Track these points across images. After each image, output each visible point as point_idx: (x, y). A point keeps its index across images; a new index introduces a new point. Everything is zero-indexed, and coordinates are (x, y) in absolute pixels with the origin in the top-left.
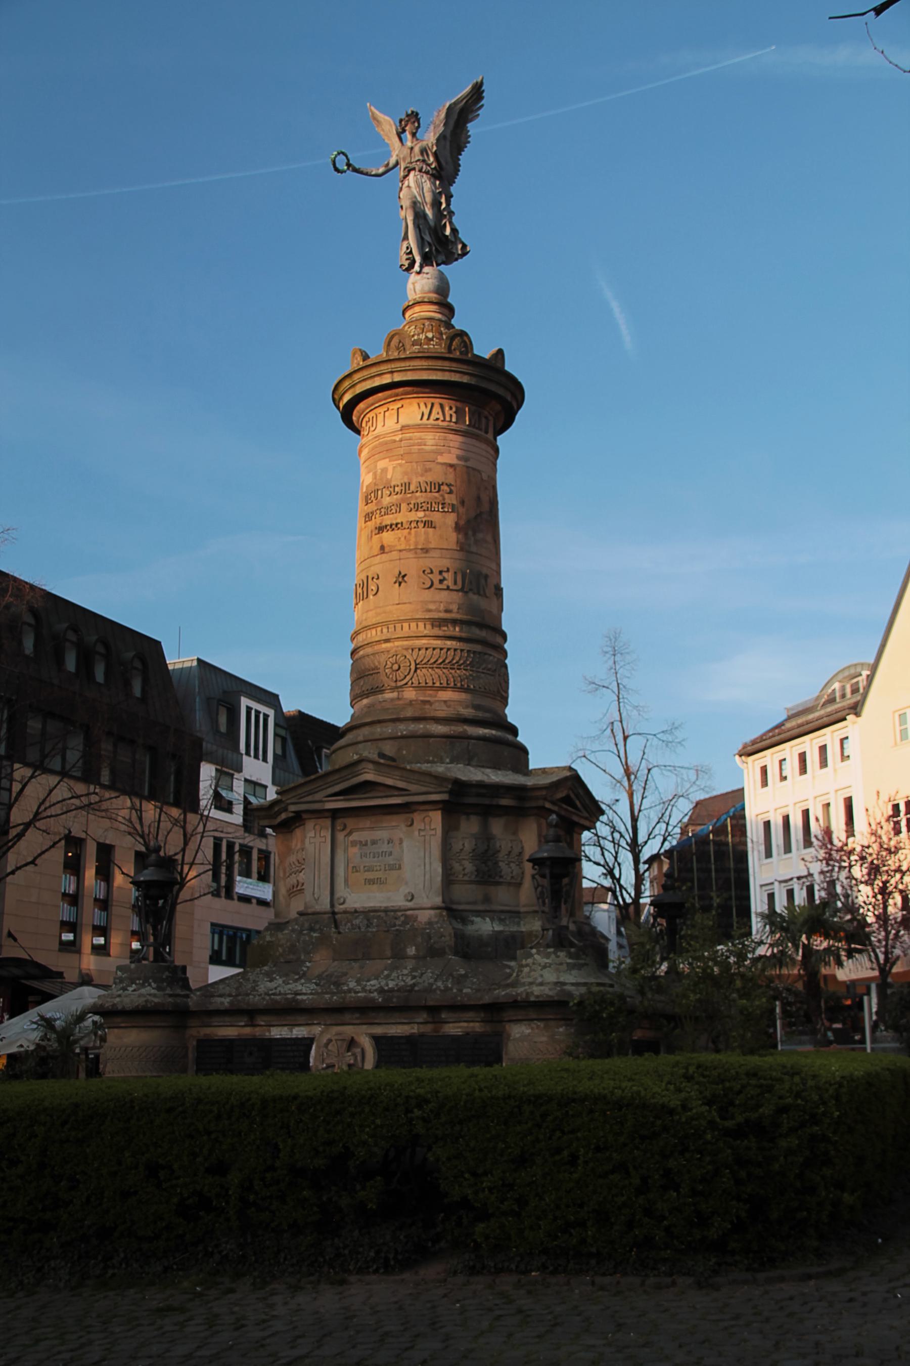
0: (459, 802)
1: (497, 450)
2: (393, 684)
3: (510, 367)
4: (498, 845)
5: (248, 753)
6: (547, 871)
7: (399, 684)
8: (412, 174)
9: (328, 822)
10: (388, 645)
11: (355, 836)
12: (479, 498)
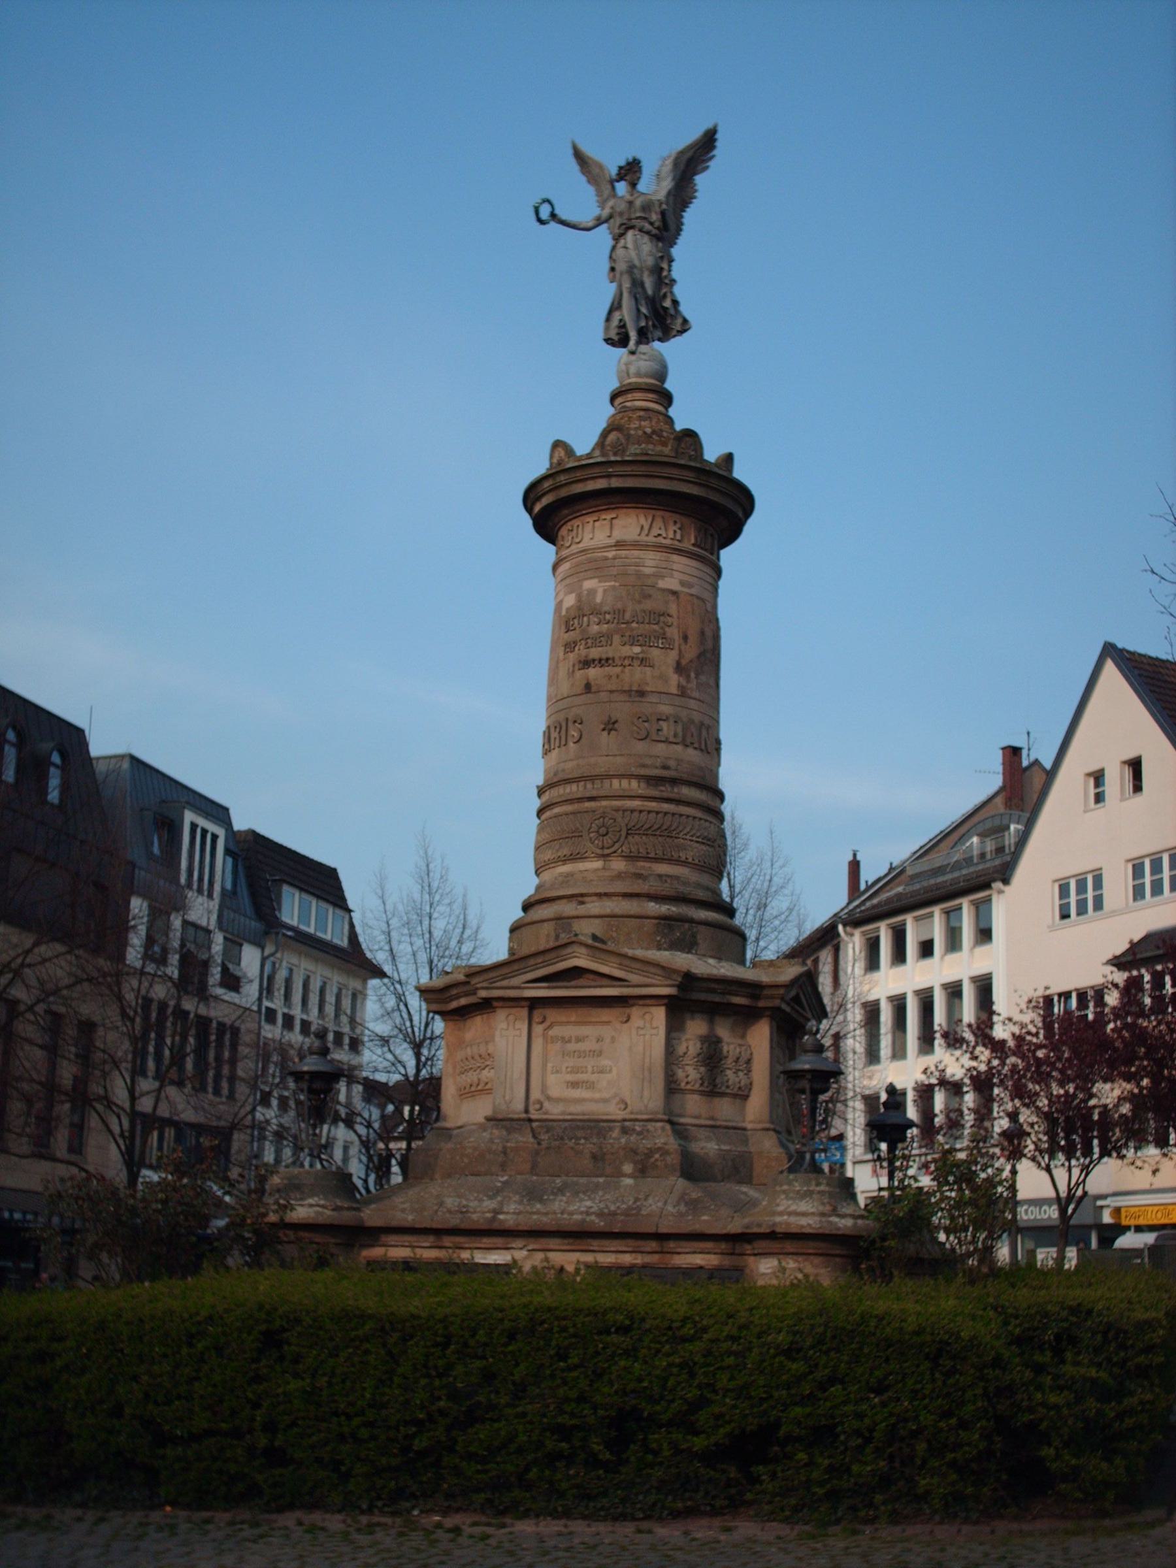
0: (688, 1000)
1: (718, 572)
2: (599, 852)
3: (740, 473)
4: (725, 1049)
5: (200, 891)
6: (305, 1086)
7: (606, 852)
8: (630, 234)
9: (524, 1012)
10: (592, 804)
11: (556, 1031)
12: (702, 633)
